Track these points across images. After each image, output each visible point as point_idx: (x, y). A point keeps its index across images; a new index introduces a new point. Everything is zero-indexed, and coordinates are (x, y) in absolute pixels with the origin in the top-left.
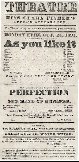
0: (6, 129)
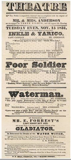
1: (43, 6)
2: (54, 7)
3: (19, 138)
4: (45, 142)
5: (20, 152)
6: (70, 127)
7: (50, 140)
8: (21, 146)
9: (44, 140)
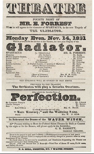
0: (16, 87)
1: (54, 7)
2: (69, 10)
3: (25, 125)
4: (58, 131)
5: (27, 144)
6: (92, 29)
7: (65, 127)
8: (27, 136)
9: (58, 128)
